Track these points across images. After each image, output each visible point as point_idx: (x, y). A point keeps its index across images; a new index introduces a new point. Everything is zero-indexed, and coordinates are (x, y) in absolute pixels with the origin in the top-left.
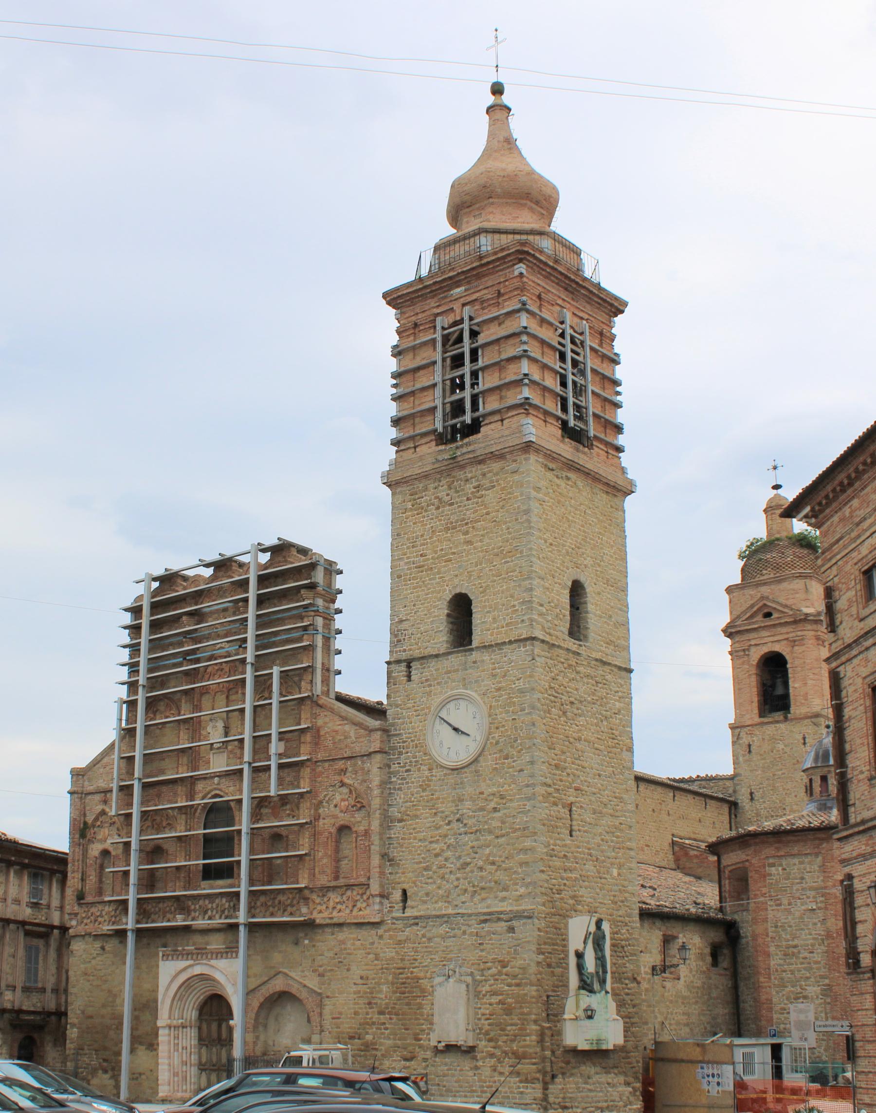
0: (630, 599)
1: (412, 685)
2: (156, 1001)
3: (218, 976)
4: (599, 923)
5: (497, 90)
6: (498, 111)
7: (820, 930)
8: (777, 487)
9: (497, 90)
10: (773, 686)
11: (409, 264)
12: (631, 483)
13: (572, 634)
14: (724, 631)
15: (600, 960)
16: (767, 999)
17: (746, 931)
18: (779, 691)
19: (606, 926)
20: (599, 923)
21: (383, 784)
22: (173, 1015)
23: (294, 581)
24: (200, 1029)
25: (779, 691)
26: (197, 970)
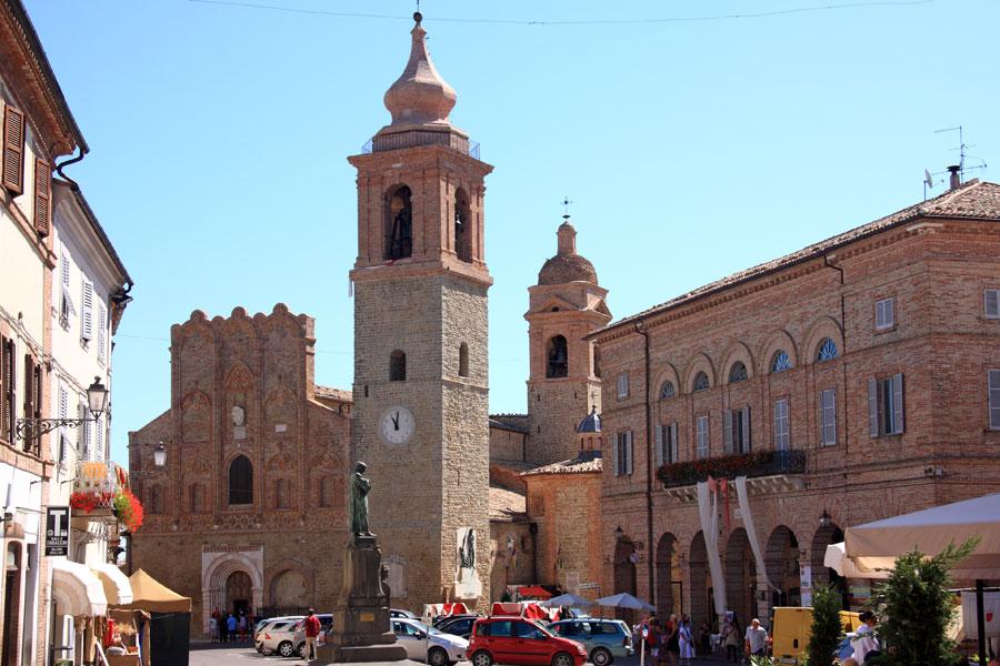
0: (489, 349)
1: (368, 399)
2: (200, 576)
3: (245, 561)
4: (471, 531)
5: (418, 17)
6: (418, 36)
7: (585, 530)
8: (566, 217)
9: (418, 17)
10: (556, 357)
11: (361, 144)
12: (492, 278)
13: (461, 374)
14: (525, 316)
15: (471, 551)
16: (624, 577)
17: (541, 528)
18: (560, 361)
19: (474, 533)
20: (471, 531)
21: (351, 453)
22: (576, 580)
23: (286, 332)
24: (228, 591)
25: (560, 361)
26: (230, 557)
